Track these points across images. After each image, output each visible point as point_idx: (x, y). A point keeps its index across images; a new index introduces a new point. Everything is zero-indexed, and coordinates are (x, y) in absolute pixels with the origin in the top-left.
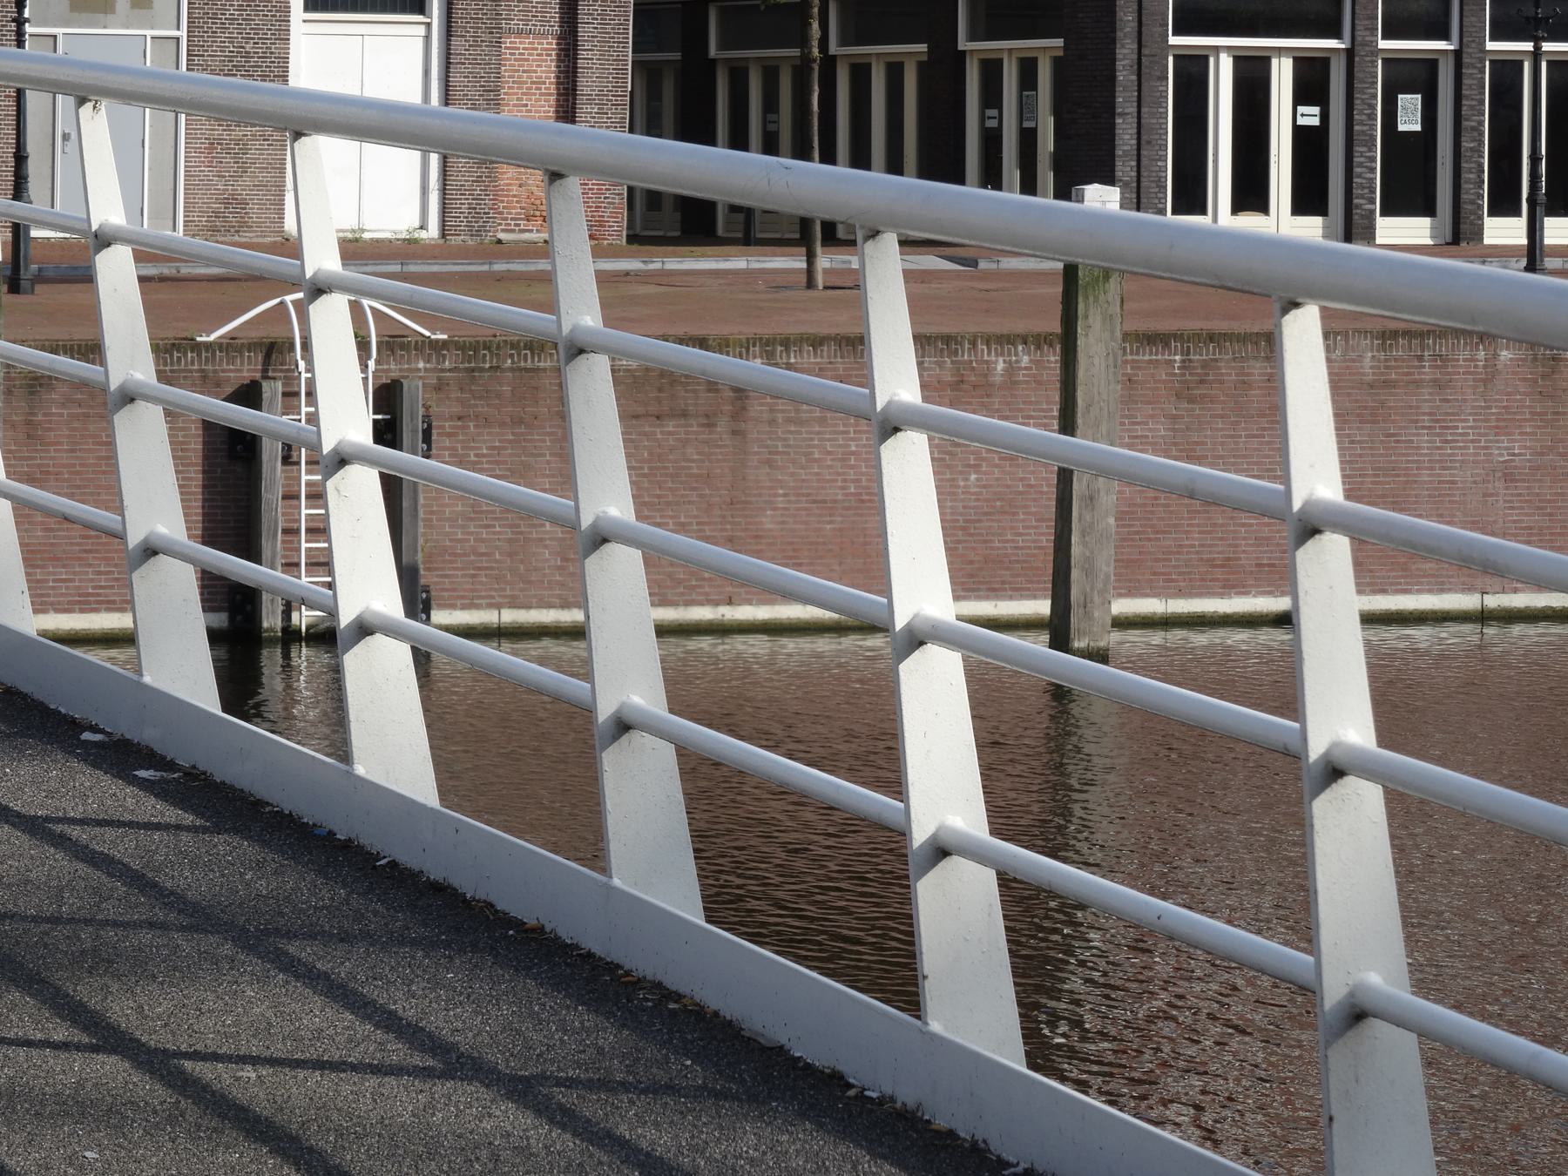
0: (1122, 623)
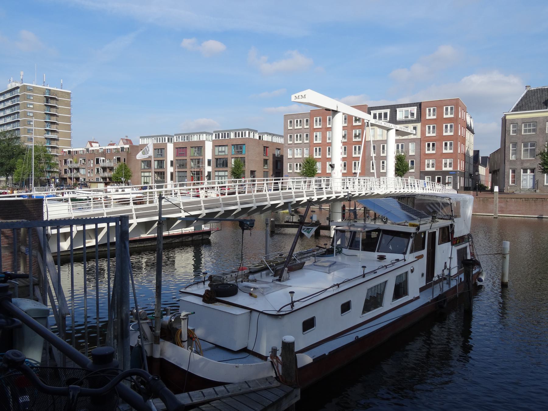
0: (498, 216)
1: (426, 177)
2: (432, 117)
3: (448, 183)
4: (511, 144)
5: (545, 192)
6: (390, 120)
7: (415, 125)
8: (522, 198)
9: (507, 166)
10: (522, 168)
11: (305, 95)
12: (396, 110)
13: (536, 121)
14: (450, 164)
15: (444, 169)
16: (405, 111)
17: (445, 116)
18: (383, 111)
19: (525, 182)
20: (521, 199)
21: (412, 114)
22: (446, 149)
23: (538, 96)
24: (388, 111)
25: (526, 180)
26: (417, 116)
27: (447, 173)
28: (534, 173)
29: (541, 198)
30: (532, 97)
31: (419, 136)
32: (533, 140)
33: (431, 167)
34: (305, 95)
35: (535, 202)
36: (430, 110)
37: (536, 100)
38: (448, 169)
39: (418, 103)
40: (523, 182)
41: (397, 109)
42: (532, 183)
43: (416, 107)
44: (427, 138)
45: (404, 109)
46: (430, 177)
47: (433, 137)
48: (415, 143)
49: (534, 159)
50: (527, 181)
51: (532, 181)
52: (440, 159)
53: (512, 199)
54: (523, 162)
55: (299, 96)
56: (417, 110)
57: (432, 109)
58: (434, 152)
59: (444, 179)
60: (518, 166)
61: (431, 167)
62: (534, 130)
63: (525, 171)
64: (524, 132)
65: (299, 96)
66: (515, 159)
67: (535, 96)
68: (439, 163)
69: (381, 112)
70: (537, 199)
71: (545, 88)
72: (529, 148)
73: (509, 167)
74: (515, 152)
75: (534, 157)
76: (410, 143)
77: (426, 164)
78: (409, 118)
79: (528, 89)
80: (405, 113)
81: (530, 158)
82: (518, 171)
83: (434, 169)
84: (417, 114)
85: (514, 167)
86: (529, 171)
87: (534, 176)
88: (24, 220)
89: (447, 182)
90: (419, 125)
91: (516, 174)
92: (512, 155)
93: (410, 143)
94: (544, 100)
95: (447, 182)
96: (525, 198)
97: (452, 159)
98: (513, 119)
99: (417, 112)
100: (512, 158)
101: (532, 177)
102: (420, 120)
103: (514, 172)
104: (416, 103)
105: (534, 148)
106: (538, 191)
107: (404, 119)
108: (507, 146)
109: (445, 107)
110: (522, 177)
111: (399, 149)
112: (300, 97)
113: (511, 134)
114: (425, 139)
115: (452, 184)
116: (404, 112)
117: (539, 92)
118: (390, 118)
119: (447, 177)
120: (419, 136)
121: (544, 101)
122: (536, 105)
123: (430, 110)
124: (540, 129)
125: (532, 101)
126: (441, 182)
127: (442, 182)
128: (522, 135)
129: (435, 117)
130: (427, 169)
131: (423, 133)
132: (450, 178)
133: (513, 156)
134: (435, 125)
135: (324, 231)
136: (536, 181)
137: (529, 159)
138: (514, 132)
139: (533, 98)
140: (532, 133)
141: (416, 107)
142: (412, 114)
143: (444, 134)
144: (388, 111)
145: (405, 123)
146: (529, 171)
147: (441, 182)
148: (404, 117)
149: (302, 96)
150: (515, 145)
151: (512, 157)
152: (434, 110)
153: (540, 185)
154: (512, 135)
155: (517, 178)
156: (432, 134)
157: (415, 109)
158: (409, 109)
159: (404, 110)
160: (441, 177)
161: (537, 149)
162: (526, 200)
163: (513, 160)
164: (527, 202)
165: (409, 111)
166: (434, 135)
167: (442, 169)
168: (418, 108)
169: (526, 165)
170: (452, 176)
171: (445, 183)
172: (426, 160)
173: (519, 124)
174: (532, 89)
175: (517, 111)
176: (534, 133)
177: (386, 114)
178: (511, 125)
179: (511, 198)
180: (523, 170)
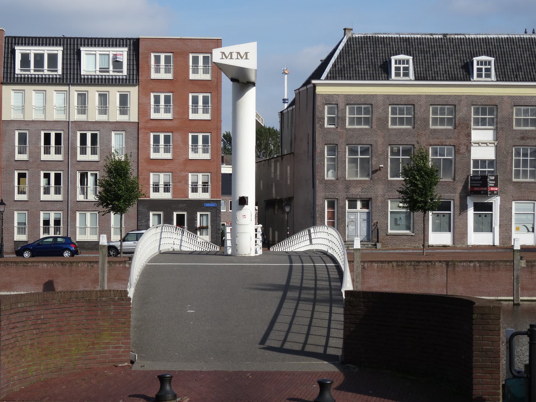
0: (522, 300)
1: (151, 214)
2: (163, 75)
3: (202, 228)
4: (326, 147)
5: (390, 247)
6: (63, 73)
7: (124, 89)
8: (391, 262)
9: (320, 193)
10: (347, 198)
11: (246, 53)
12: (79, 53)
13: (370, 102)
14: (205, 184)
15: (192, 196)
16: (100, 54)
17: (192, 76)
18: (46, 50)
19: (354, 227)
20: (391, 264)
21: (117, 64)
22: (195, 150)
23: (370, 52)
24: (59, 51)
25: (354, 222)
26: (129, 69)
27: (199, 205)
28: (368, 208)
29: (426, 262)
30: (358, 52)
31: (133, 116)
32: (366, 140)
33: (200, 190)
34: (246, 53)
35: (415, 269)
36: (158, 59)
37: (367, 61)
38: (200, 195)
39: (130, 39)
40: (350, 227)
41: (82, 49)
42: (365, 229)
43: (126, 49)
44: (153, 124)
45: (99, 50)
46: (161, 213)
47: (166, 122)
48: (124, 133)
49: (367, 179)
50: (356, 226)
51: (364, 225)
52: (183, 174)
53: (374, 264)
54: (348, 185)
55: (231, 53)
56: (129, 55)
57: (163, 56)
58: (169, 156)
59: (192, 220)
60: (340, 194)
61: (200, 190)
62: (367, 121)
63: (353, 206)
64: (350, 124)
65: (231, 53)
66: (333, 178)
67: (364, 52)
68: (180, 182)
69: (42, 52)
70: (419, 262)
71: (379, 36)
72: (359, 156)
73: (323, 194)
74: (336, 165)
75: (368, 176)
76: (113, 133)
77: (151, 183)
78: (111, 73)
79: (349, 35)
80: (101, 60)
81: (361, 176)
82: (341, 204)
83: (168, 196)
84: (129, 64)
85: (332, 195)
86: (359, 204)
87: (368, 213)
88: (121, 365)
89: (198, 225)
90: (133, 92)
91: (336, 210)
92: (328, 171)
93: (113, 133)
94: (381, 60)
95: (198, 225)
96: (397, 262)
97: (209, 174)
98: (329, 95)
99: (129, 60)
100: (327, 177)
101: (365, 216)
102: (138, 80)
103: (331, 205)
104: (127, 39)
105: (493, 170)
106: (379, 245)
107: (98, 73)
108: (318, 150)
109: (191, 56)
110: (348, 216)
111: (85, 144)
112: (235, 55)
113: (326, 126)
114: (149, 125)
115: (209, 230)
116: (98, 56)
117: (369, 43)
118: (63, 69)
119: (199, 214)
120: (133, 116)
121: (382, 63)
122: (368, 69)
123: (158, 59)
124: (379, 119)
125: (359, 60)
126: (186, 226)
127: (188, 226)
128: (346, 129)
129: (170, 76)
130: (153, 196)
131: (143, 110)
132: (205, 217)
133: (330, 172)
134: (171, 94)
135: (526, 347)
136: (374, 225)
137: (359, 178)
138: (331, 121)
139: (361, 54)
140: (363, 127)
141: (126, 49)
142: (117, 64)
143: (192, 116)
144: (59, 51)
145: (102, 85)
146: (359, 204)
147: (186, 226)
148: (98, 69)
149: (238, 53)
150: (333, 149)
151: (329, 176)
152: (167, 59)
153: (381, 234)
154: (329, 128)
155: (338, 220)
156: (162, 115)
157: (123, 54)
158: (112, 51)
159: (98, 53)
160: (185, 213)
161: (374, 159)
162: (398, 266)
163: (331, 181)
164: (400, 268)
165: (111, 56)
166: (169, 116)
167: (188, 197)
168: (129, 50)
169: (356, 191)
170: (209, 213)
171: (193, 229)
172: (151, 174)
173: (341, 105)
174: (357, 36)
175: (336, 79)
176: (367, 127)
177: (53, 58)
178: (326, 107)
179: (372, 262)
180: (349, 201)
